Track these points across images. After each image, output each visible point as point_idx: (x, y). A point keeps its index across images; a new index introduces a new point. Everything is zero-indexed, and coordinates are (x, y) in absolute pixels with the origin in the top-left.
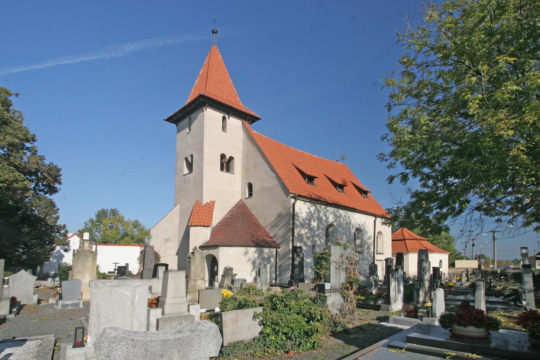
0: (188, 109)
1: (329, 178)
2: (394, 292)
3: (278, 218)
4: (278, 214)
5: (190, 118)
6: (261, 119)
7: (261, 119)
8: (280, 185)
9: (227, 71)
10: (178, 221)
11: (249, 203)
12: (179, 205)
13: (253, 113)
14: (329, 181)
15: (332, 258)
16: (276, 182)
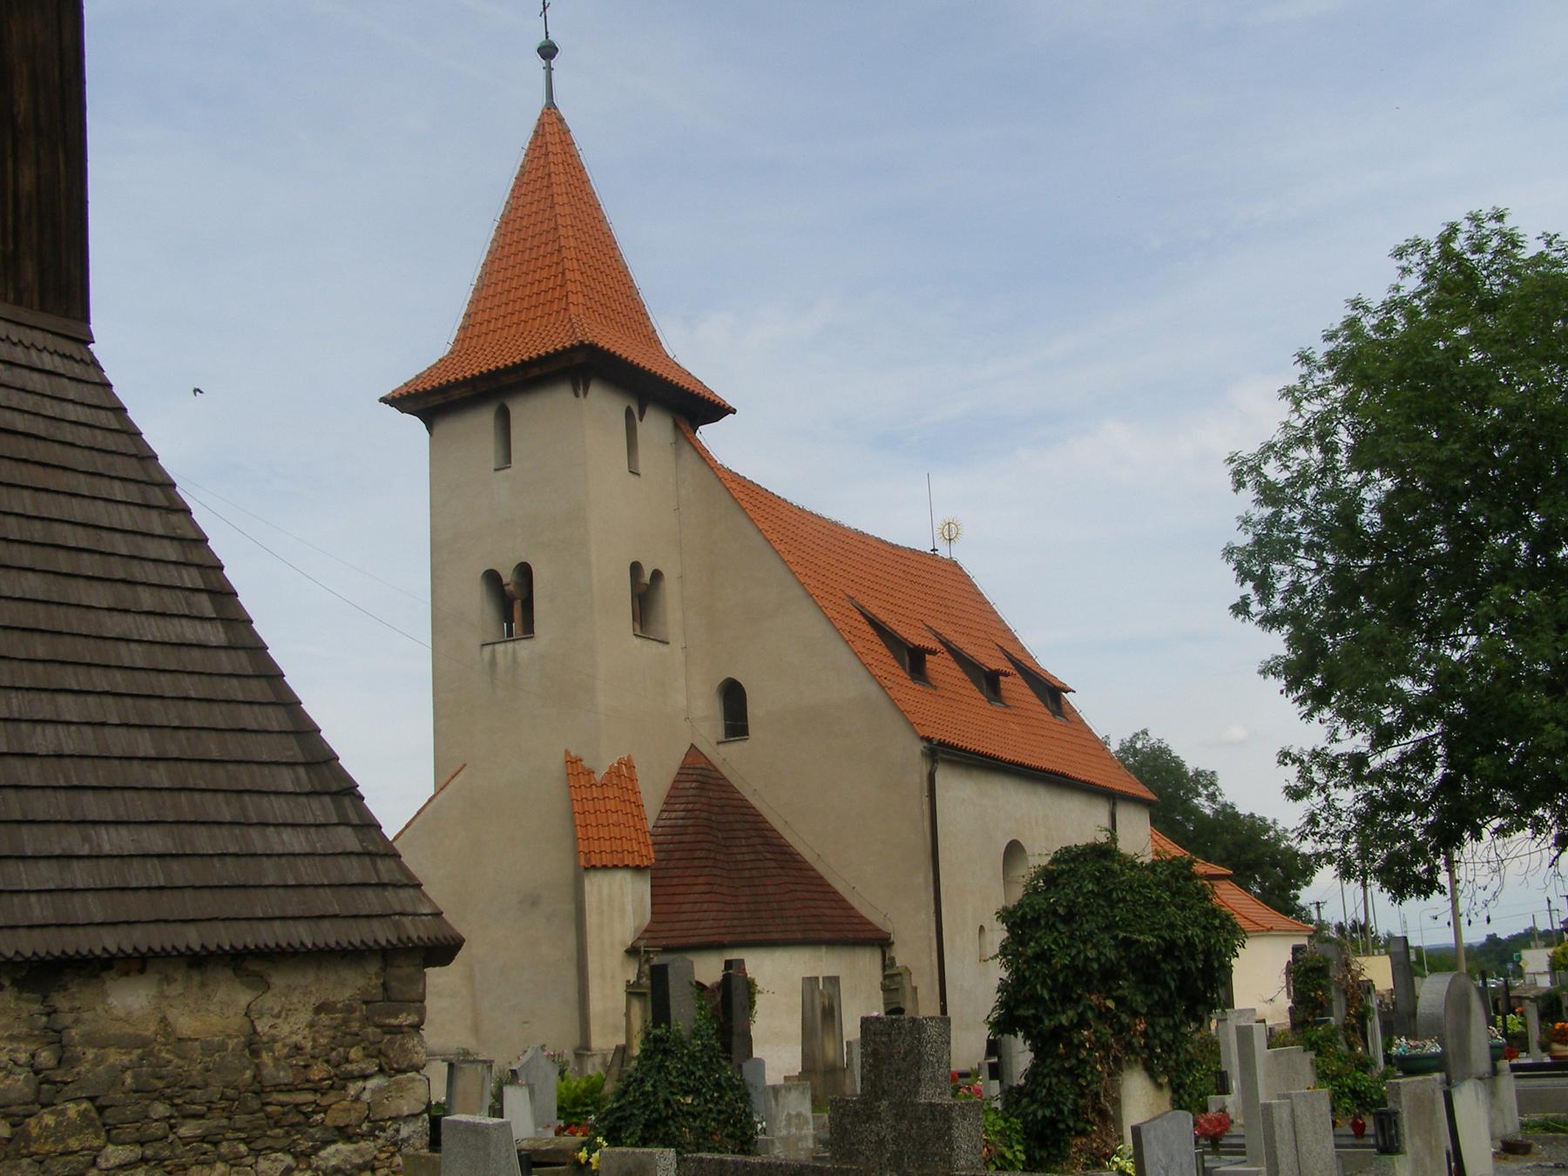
11: (733, 760)
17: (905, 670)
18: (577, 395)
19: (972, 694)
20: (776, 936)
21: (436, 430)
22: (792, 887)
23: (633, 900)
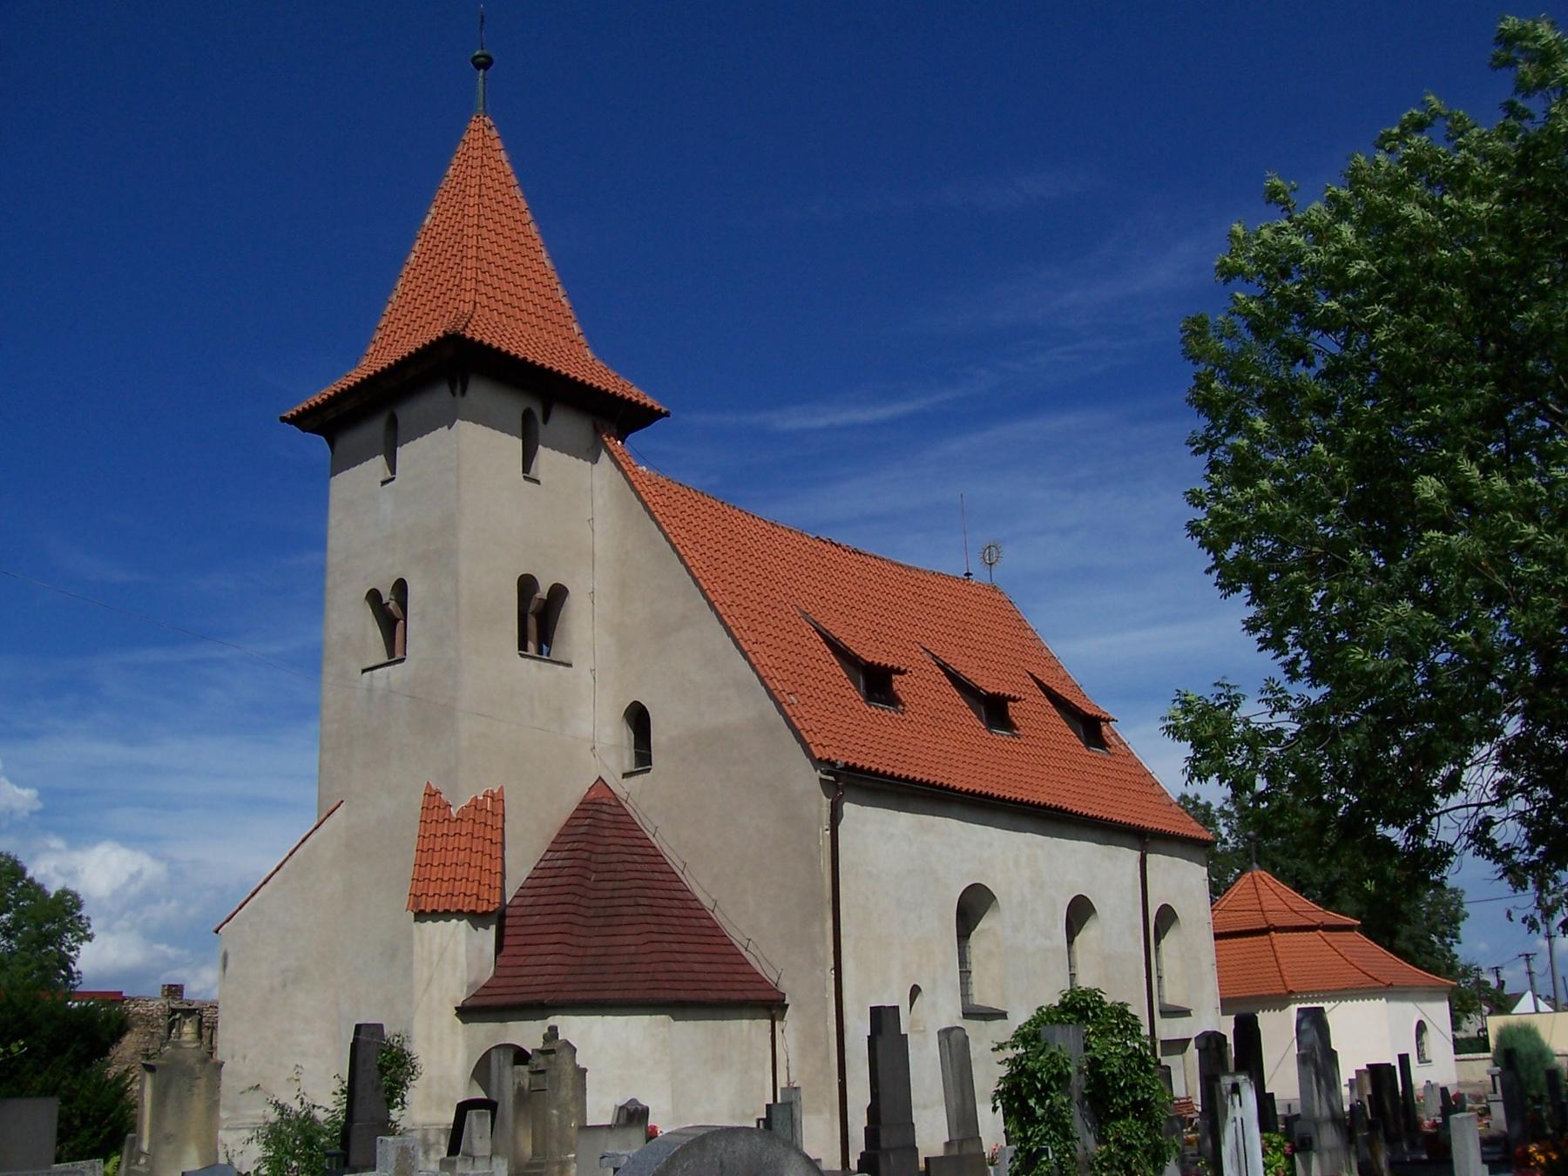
1: (944, 667)
2: (1236, 1168)
5: (393, 423)
6: (667, 414)
7: (667, 414)
9: (528, 217)
11: (640, 796)
13: (634, 393)
14: (945, 680)
17: (859, 692)
18: (454, 394)
19: (970, 720)
20: (608, 995)
21: (338, 448)
22: (655, 937)
23: (467, 951)
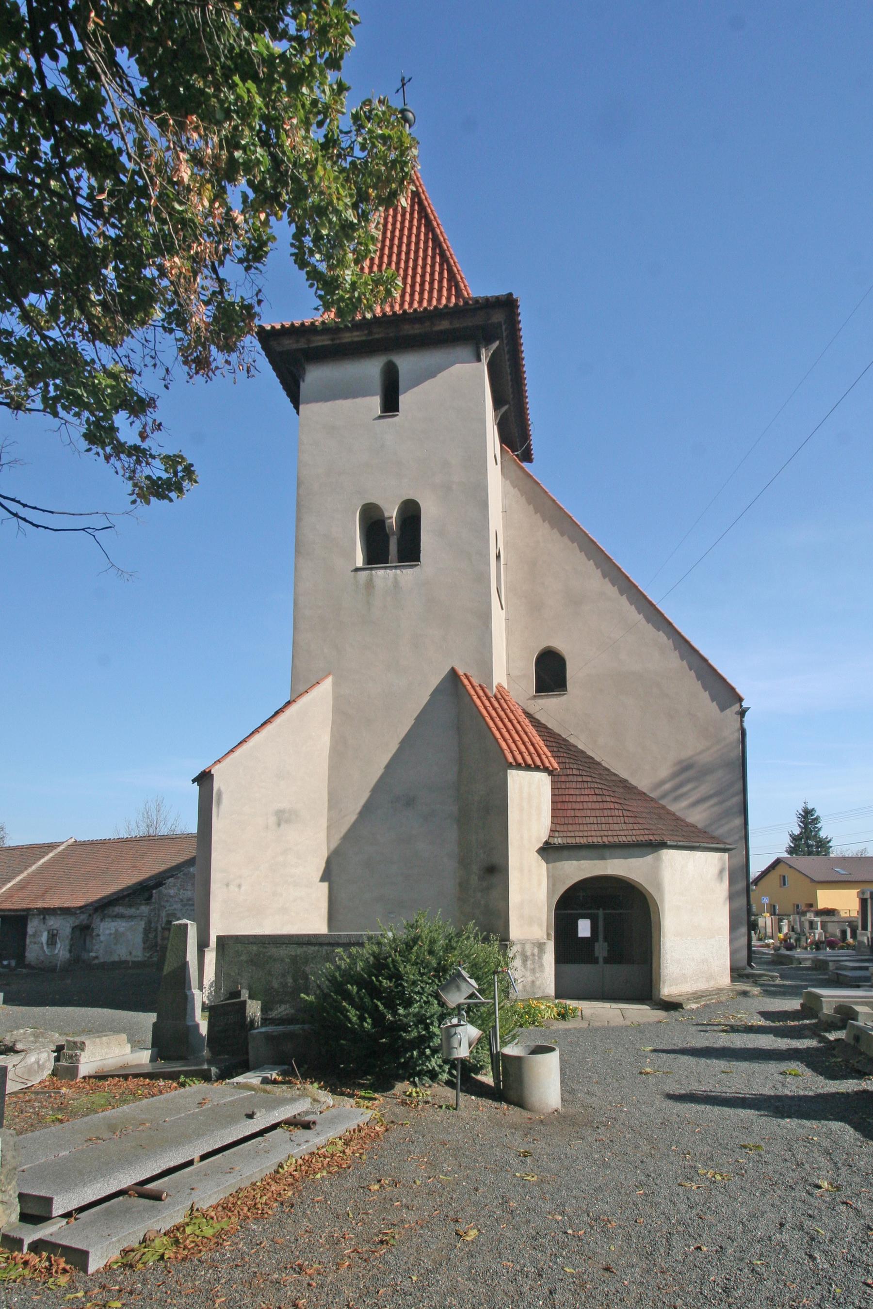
0: (408, 329)
3: (674, 775)
4: (680, 762)
8: (692, 673)
10: (328, 744)
12: (328, 684)
15: (293, 953)
16: (675, 661)
